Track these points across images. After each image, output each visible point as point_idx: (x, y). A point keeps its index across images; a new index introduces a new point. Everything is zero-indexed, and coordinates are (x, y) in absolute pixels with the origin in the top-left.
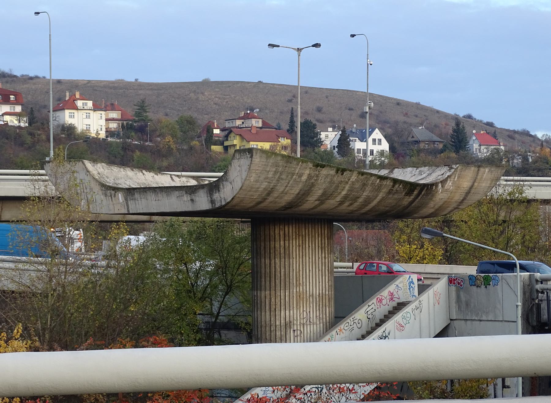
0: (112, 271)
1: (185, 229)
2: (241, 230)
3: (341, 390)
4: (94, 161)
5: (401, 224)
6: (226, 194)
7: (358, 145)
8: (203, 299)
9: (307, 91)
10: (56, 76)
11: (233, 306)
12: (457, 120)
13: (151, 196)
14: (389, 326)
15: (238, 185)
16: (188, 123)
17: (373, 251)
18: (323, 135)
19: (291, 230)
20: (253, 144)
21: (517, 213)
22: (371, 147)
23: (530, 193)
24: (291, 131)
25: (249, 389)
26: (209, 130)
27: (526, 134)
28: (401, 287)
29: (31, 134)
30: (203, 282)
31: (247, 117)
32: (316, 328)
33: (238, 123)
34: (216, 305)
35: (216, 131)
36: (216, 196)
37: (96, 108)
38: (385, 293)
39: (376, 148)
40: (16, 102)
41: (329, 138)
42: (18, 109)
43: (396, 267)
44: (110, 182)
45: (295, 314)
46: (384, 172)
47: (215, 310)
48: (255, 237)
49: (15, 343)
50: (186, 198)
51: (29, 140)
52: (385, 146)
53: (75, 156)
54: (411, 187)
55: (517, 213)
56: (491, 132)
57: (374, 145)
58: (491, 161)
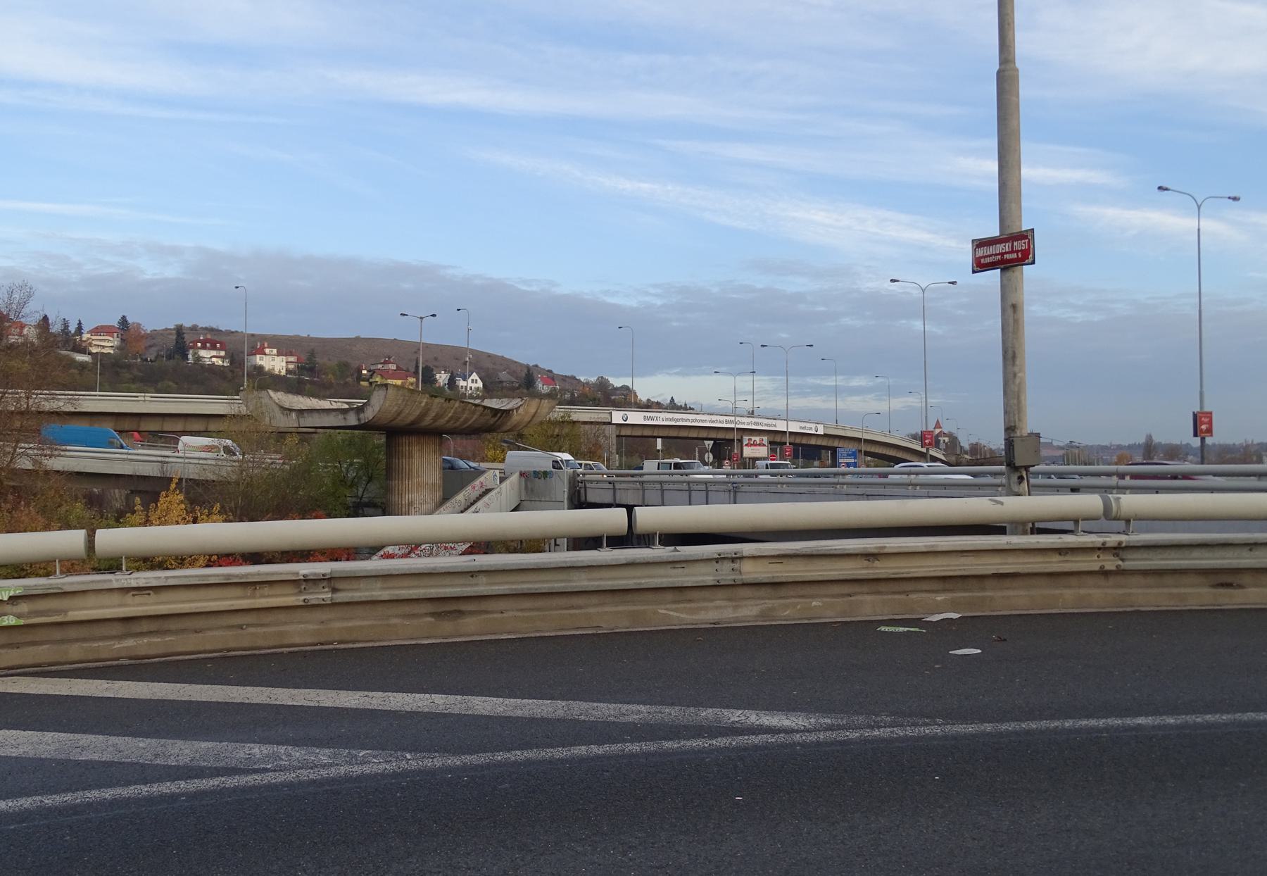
0: (287, 467)
1: (339, 438)
2: (380, 439)
3: (446, 548)
4: (276, 390)
5: (489, 436)
6: (369, 414)
7: (462, 383)
8: (351, 486)
9: (427, 346)
10: (250, 331)
11: (373, 490)
12: (528, 367)
13: (316, 415)
14: (479, 504)
15: (377, 409)
16: (344, 366)
17: (470, 454)
18: (438, 376)
19: (413, 439)
20: (390, 381)
21: (566, 430)
22: (470, 384)
23: (575, 417)
24: (416, 373)
25: (383, 547)
26: (359, 371)
27: (574, 378)
28: (488, 479)
29: (232, 371)
30: (352, 474)
31: (385, 363)
32: (430, 506)
33: (380, 366)
34: (361, 490)
35: (364, 372)
36: (362, 416)
37: (279, 354)
38: (477, 482)
39: (474, 386)
40: (221, 349)
41: (442, 378)
42: (223, 353)
43: (484, 465)
44: (287, 405)
45: (415, 496)
46: (477, 402)
47: (360, 493)
48: (389, 444)
49: (215, 517)
50: (341, 417)
51: (230, 375)
52: (480, 384)
53: (263, 387)
54: (495, 412)
55: (566, 430)
56: (550, 377)
57: (473, 383)
58: (550, 396)
